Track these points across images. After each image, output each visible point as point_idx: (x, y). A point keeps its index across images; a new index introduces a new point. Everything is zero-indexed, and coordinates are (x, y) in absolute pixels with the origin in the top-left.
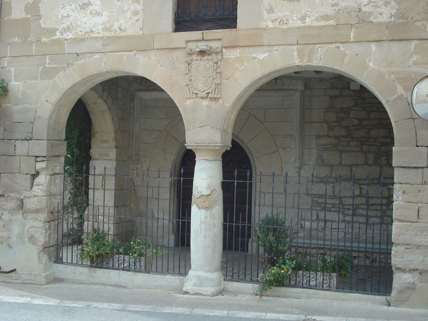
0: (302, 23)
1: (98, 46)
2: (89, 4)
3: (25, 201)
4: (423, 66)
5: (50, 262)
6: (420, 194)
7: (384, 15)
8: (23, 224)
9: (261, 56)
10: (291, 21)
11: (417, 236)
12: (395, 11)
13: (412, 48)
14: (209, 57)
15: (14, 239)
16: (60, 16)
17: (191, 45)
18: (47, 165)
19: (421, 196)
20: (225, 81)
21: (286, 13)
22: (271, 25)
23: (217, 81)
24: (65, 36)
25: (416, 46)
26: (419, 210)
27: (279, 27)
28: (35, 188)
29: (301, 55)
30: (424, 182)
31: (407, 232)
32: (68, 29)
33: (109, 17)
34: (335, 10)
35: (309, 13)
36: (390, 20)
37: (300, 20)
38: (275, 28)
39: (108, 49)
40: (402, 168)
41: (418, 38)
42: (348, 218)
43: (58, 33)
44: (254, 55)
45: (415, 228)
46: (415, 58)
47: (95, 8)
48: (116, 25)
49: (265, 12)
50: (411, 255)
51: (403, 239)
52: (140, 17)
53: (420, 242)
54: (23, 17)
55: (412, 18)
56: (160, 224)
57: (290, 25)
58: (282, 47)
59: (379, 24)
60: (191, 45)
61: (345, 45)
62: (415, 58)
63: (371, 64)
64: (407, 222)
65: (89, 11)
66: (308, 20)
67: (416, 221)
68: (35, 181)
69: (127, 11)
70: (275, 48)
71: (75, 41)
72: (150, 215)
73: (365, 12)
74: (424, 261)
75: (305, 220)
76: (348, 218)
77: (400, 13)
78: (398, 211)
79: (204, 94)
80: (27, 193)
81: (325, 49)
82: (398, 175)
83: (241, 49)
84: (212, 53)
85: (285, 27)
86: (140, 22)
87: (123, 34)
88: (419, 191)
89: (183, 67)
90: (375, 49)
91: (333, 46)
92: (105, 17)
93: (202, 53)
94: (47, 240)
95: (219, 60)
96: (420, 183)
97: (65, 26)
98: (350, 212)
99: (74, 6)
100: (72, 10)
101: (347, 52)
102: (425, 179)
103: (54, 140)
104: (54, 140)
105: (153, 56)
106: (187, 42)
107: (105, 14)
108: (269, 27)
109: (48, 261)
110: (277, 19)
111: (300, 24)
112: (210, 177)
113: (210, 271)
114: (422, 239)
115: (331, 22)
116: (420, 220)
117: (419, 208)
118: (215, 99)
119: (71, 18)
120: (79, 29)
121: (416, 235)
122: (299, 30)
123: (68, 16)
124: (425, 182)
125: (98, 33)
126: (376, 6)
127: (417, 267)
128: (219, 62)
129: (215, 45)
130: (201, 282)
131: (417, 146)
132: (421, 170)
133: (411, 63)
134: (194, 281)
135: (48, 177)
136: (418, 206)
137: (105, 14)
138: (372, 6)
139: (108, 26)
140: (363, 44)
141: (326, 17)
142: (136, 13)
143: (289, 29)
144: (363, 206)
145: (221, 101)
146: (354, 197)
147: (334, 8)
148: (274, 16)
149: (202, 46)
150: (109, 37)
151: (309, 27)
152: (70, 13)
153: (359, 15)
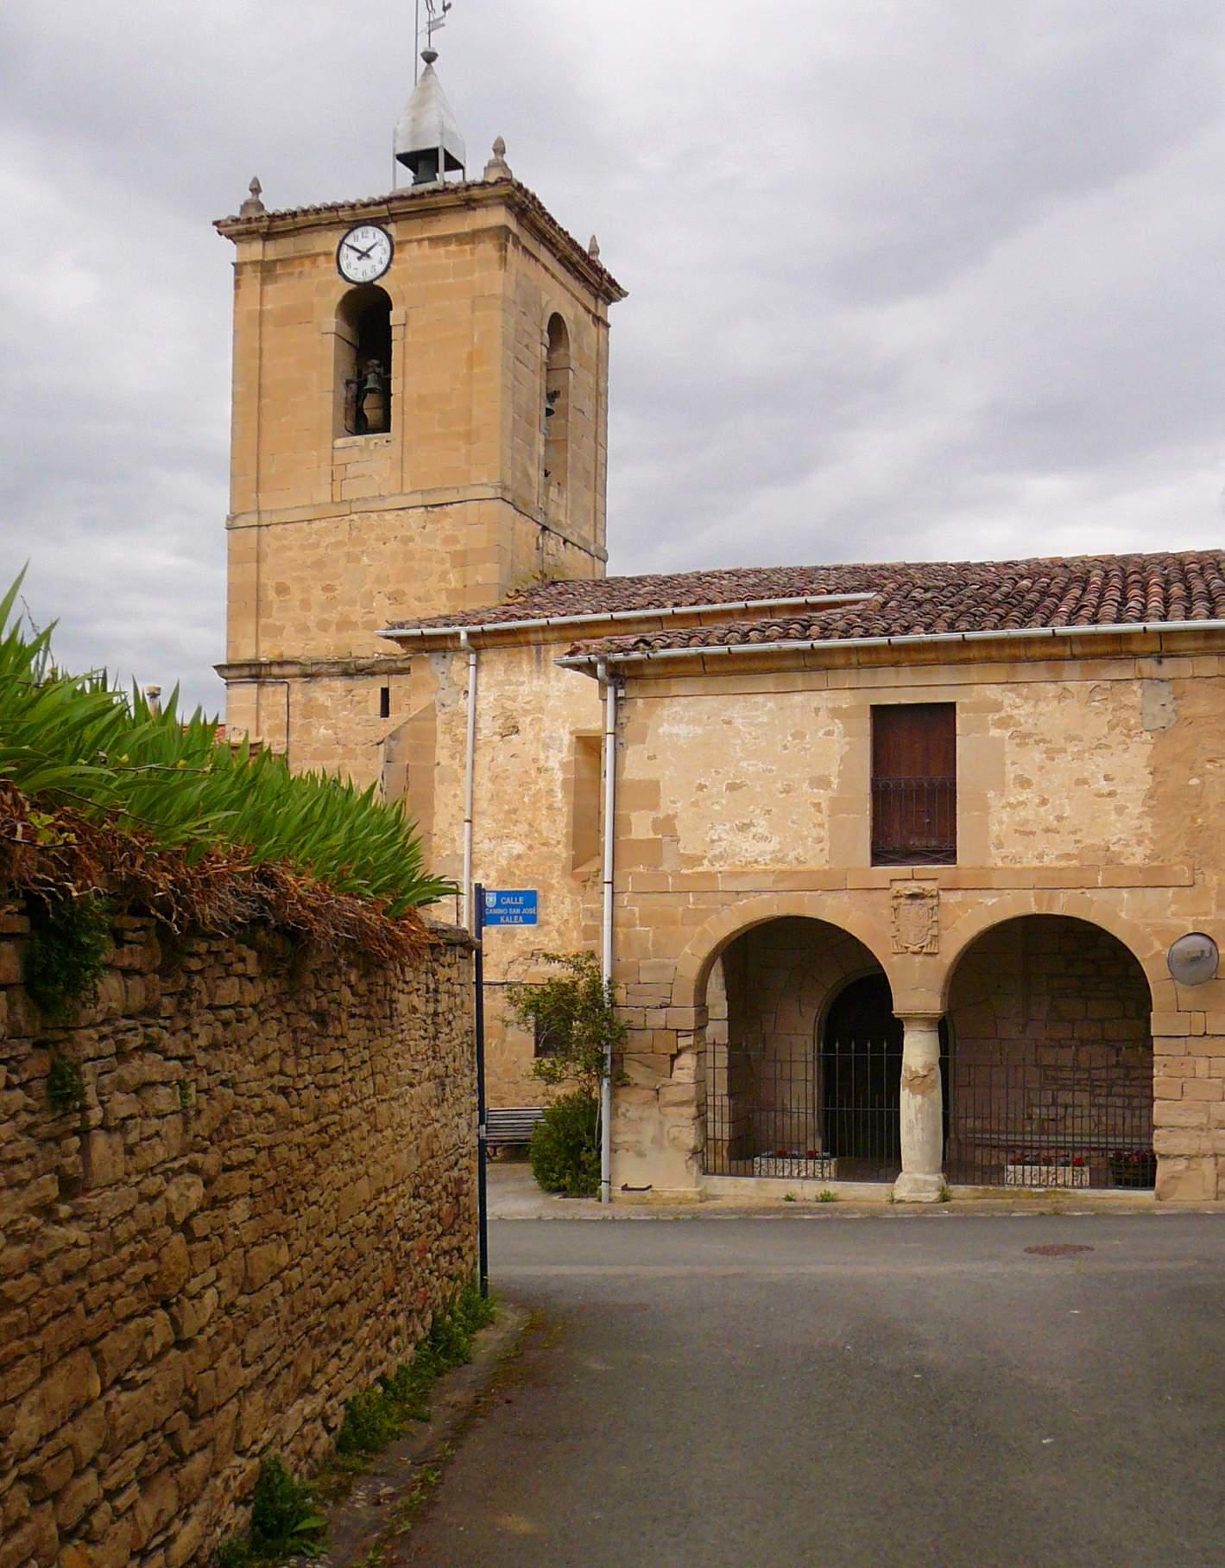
1: (767, 883)
2: (751, 824)
3: (661, 1091)
8: (661, 1123)
9: (990, 902)
14: (922, 902)
15: (647, 1143)
16: (708, 839)
17: (897, 886)
20: (943, 932)
21: (1020, 849)
22: (1000, 864)
24: (717, 867)
28: (676, 1073)
29: (1038, 902)
32: (720, 857)
38: (1006, 869)
39: (780, 887)
42: (1101, 1100)
43: (706, 862)
46: (1173, 908)
47: (760, 830)
48: (792, 855)
49: (992, 848)
52: (826, 845)
56: (795, 1121)
57: (1025, 865)
60: (897, 886)
62: (1173, 908)
63: (1123, 915)
65: (751, 835)
68: (676, 1062)
69: (806, 837)
71: (733, 875)
72: (779, 1106)
73: (1114, 852)
75: (1032, 1105)
76: (1101, 1100)
79: (916, 949)
80: (665, 1080)
82: (1157, 1046)
85: (1018, 866)
86: (826, 852)
87: (801, 868)
89: (886, 912)
92: (774, 845)
93: (913, 896)
97: (717, 852)
98: (1104, 1092)
99: (728, 826)
100: (725, 831)
105: (844, 897)
107: (775, 840)
111: (1036, 863)
113: (928, 1173)
115: (1074, 863)
119: (723, 844)
120: (736, 859)
123: (720, 839)
125: (766, 864)
126: (1127, 845)
129: (929, 886)
130: (921, 1186)
133: (1169, 913)
134: (909, 1187)
137: (775, 840)
139: (780, 855)
141: (1068, 856)
142: (819, 840)
143: (1024, 869)
144: (1121, 1082)
145: (938, 957)
146: (1108, 1068)
148: (1004, 852)
149: (913, 887)
150: (783, 872)
151: (1048, 868)
152: (723, 835)
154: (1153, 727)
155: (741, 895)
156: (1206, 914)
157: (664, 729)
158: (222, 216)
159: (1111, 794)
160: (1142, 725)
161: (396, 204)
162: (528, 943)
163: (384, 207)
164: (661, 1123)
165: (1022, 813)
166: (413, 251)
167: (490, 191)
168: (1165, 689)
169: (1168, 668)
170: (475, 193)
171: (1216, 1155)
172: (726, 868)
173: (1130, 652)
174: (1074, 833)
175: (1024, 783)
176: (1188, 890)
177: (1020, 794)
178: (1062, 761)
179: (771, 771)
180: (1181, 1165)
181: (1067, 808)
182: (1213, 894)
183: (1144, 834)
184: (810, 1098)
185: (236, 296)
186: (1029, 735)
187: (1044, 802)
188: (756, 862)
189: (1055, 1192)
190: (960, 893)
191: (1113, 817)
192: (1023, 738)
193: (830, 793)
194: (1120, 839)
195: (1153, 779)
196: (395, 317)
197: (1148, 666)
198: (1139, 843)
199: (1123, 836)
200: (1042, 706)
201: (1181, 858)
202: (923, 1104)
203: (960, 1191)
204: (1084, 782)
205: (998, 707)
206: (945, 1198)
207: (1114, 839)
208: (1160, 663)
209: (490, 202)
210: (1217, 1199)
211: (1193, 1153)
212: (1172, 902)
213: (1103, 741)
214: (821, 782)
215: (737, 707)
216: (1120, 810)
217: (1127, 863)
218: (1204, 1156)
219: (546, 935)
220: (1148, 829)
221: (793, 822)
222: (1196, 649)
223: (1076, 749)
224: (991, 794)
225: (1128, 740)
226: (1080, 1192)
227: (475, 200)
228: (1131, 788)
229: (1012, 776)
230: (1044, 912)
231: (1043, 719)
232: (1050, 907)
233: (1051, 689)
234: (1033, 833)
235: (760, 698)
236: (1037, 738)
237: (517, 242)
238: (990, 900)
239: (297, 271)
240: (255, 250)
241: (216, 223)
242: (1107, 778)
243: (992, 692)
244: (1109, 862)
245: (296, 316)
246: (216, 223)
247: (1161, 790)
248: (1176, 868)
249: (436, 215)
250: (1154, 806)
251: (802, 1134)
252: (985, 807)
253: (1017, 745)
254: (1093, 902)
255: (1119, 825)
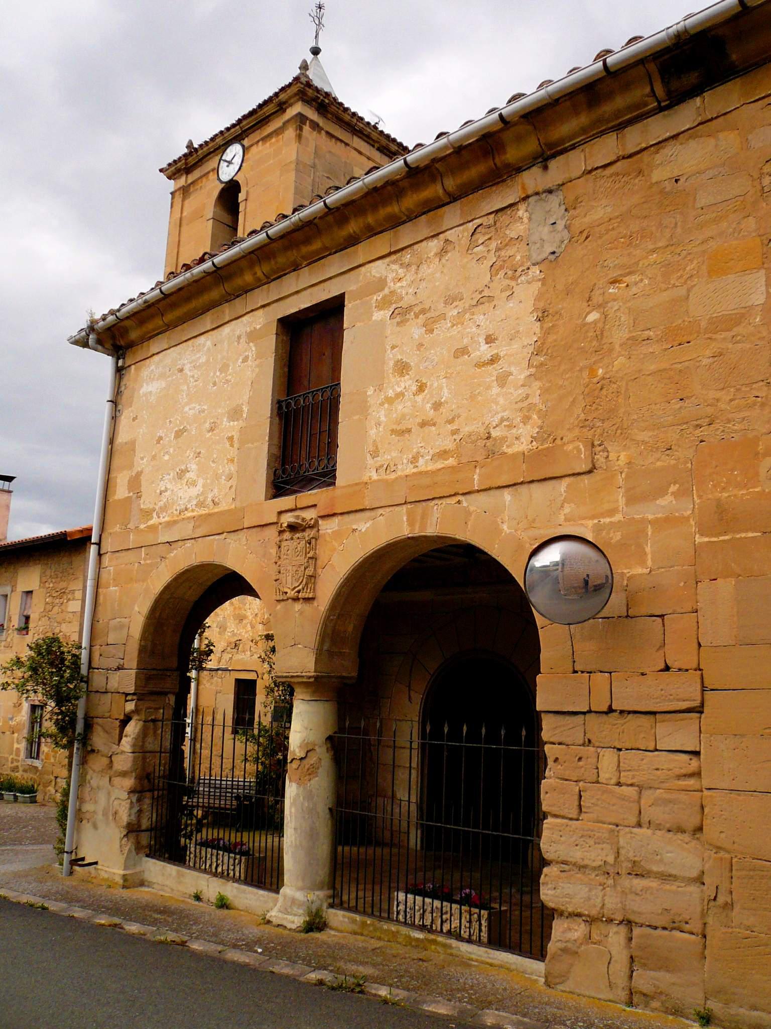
0: (414, 468)
4: (580, 522)
5: (137, 854)
6: (581, 763)
7: (523, 440)
10: (400, 467)
11: (578, 848)
12: (537, 430)
13: (562, 490)
16: (158, 491)
18: (136, 705)
19: (583, 769)
21: (394, 454)
22: (375, 477)
23: (310, 572)
25: (568, 486)
26: (580, 797)
27: (385, 477)
29: (411, 523)
30: (587, 740)
31: (562, 839)
33: (204, 486)
34: (455, 440)
35: (422, 450)
36: (530, 447)
37: (412, 463)
40: (551, 715)
41: (570, 472)
44: (355, 527)
45: (573, 831)
50: (569, 885)
51: (555, 852)
52: (233, 482)
53: (583, 859)
54: (127, 495)
55: (562, 439)
57: (399, 473)
58: (388, 510)
59: (514, 456)
61: (468, 497)
62: (567, 509)
63: (505, 527)
64: (563, 817)
66: (421, 461)
67: (575, 817)
70: (381, 511)
71: (170, 524)
73: (495, 439)
74: (589, 899)
77: (544, 432)
78: (548, 795)
81: (442, 506)
82: (549, 729)
83: (340, 517)
84: (306, 528)
85: (393, 476)
86: (233, 489)
88: (580, 759)
90: (509, 499)
91: (454, 500)
92: (199, 488)
94: (133, 817)
95: (313, 538)
96: (581, 742)
101: (472, 509)
102: (588, 736)
103: (154, 669)
104: (154, 669)
106: (280, 513)
107: (200, 482)
108: (373, 479)
109: (134, 852)
110: (383, 466)
111: (410, 470)
112: (306, 729)
114: (586, 853)
115: (451, 461)
116: (583, 816)
117: (580, 791)
118: (307, 600)
119: (168, 493)
121: (577, 845)
122: (408, 478)
123: (166, 490)
124: (589, 741)
127: (579, 911)
128: (313, 541)
129: (310, 515)
131: (575, 672)
132: (582, 716)
135: (141, 723)
136: (578, 788)
138: (505, 426)
139: (202, 498)
140: (492, 492)
141: (443, 454)
145: (315, 603)
147: (455, 437)
153: (488, 444)
154: (540, 258)
155: (174, 545)
156: (612, 512)
157: (145, 389)
158: (164, 165)
159: (493, 360)
160: (529, 258)
161: (244, 123)
162: (234, 635)
163: (238, 127)
164: (109, 793)
165: (400, 407)
166: (254, 149)
167: (290, 92)
168: (554, 201)
169: (558, 170)
170: (283, 97)
171: (629, 923)
172: (167, 519)
173: (507, 166)
174: (451, 421)
175: (402, 368)
176: (585, 478)
177: (398, 384)
178: (443, 330)
179: (203, 411)
180: (578, 930)
181: (445, 390)
182: (620, 480)
183: (531, 407)
184: (414, 787)
185: (171, 212)
186: (410, 308)
187: (421, 388)
188: (186, 509)
189: (434, 942)
190: (336, 520)
191: (495, 390)
192: (401, 314)
193: (241, 423)
194: (502, 420)
195: (542, 328)
196: (241, 197)
197: (532, 179)
198: (526, 419)
199: (506, 414)
200: (425, 270)
201: (577, 432)
202: (297, 795)
203: (338, 917)
204: (463, 351)
205: (381, 283)
206: (315, 924)
207: (496, 420)
208: (546, 168)
209: (292, 101)
210: (630, 1003)
211: (594, 912)
212: (564, 501)
213: (486, 293)
214: (235, 413)
215: (187, 353)
216: (502, 380)
217: (510, 451)
218: (610, 921)
219: (244, 628)
220: (536, 399)
221: (213, 462)
222: (584, 130)
223: (455, 312)
224: (370, 392)
225: (513, 283)
226: (465, 947)
227: (285, 103)
228: (516, 346)
229: (391, 363)
230: (417, 533)
231: (423, 285)
232: (423, 526)
233: (434, 246)
234: (409, 431)
235: (202, 339)
236: (417, 309)
237: (315, 126)
238: (363, 524)
239: (198, 187)
240: (182, 181)
241: (161, 170)
242: (490, 340)
243: (378, 269)
244: (490, 454)
245: (198, 215)
246: (161, 170)
247: (551, 338)
248: (570, 447)
249: (267, 123)
250: (542, 364)
251: (404, 824)
252: (363, 408)
253: (398, 324)
254: (469, 513)
255: (501, 401)
